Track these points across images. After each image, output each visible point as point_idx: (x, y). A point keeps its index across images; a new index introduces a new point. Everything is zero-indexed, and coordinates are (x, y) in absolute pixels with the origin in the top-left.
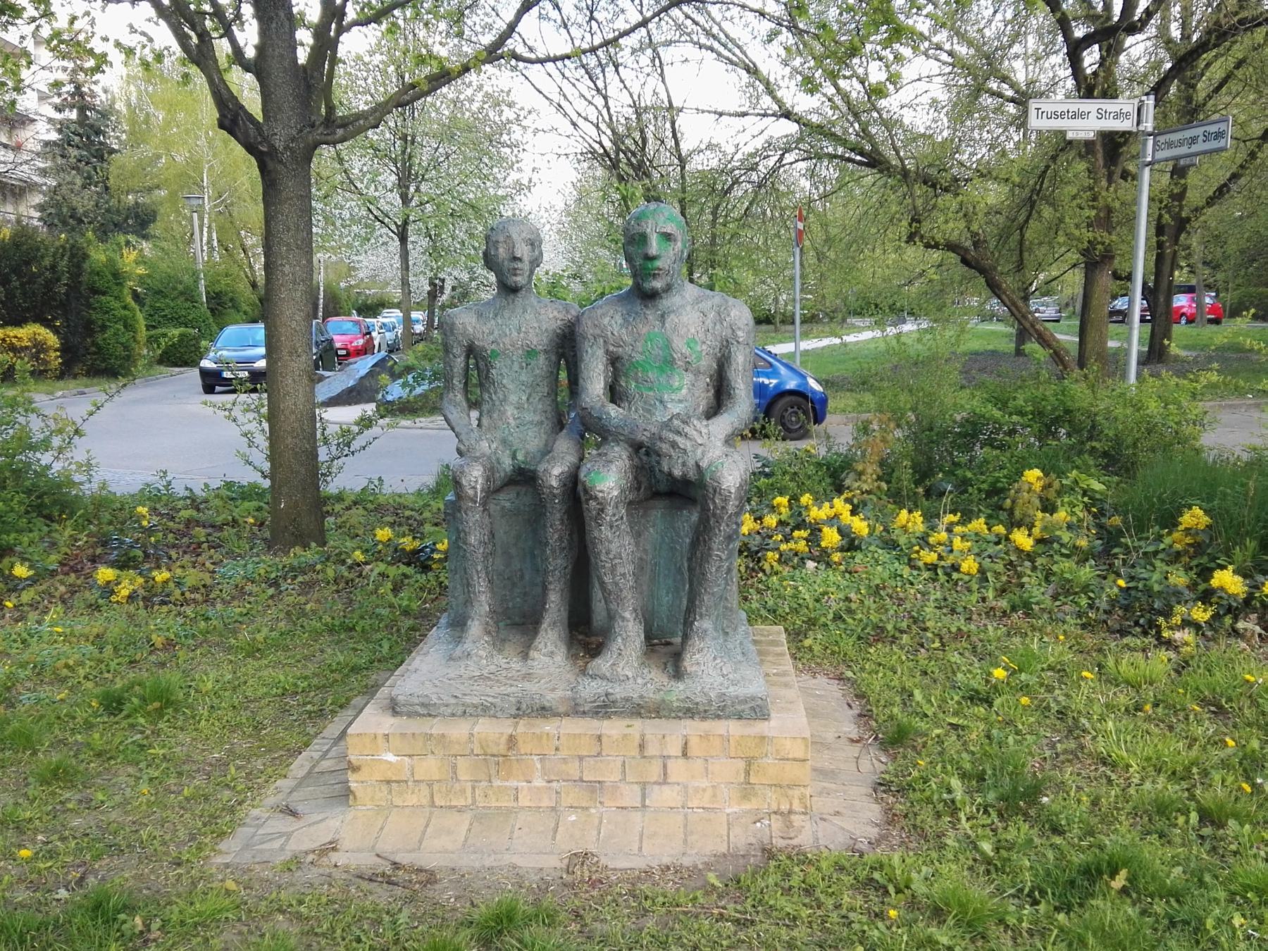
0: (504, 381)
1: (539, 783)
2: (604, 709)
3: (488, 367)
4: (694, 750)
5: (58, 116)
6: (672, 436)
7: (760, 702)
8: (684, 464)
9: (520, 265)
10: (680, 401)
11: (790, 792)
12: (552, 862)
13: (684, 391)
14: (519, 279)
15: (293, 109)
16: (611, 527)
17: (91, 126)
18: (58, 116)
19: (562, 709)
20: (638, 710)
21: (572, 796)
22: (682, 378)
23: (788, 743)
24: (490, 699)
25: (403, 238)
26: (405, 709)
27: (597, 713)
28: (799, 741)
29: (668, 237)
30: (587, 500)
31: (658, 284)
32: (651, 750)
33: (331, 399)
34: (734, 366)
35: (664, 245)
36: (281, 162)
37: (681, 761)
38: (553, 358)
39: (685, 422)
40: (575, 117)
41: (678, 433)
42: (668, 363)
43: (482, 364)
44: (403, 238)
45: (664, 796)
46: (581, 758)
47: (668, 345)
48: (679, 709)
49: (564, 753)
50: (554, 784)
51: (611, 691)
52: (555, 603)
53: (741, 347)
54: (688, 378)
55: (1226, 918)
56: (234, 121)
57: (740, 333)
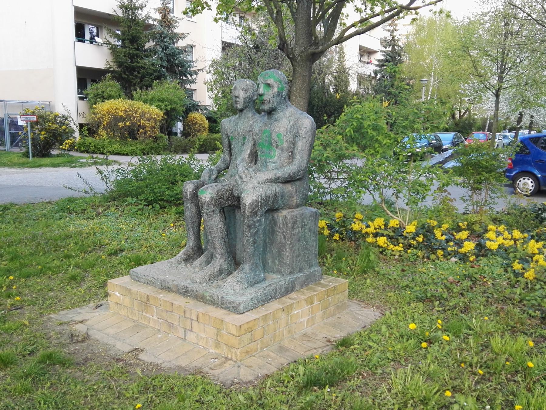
1: (155, 318)
4: (201, 320)
5: (384, 49)
9: (238, 100)
10: (274, 163)
11: (232, 350)
12: (122, 347)
13: (276, 158)
14: (238, 105)
15: (304, 39)
16: (207, 215)
17: (396, 53)
18: (384, 49)
19: (174, 290)
21: (164, 328)
22: (275, 152)
23: (230, 325)
25: (497, 96)
27: (185, 294)
28: (234, 326)
29: (269, 85)
32: (188, 315)
36: (296, 62)
37: (196, 322)
44: (497, 96)
45: (191, 337)
46: (167, 311)
47: (270, 136)
48: (208, 300)
49: (162, 308)
50: (159, 320)
54: (278, 152)
56: (283, 46)
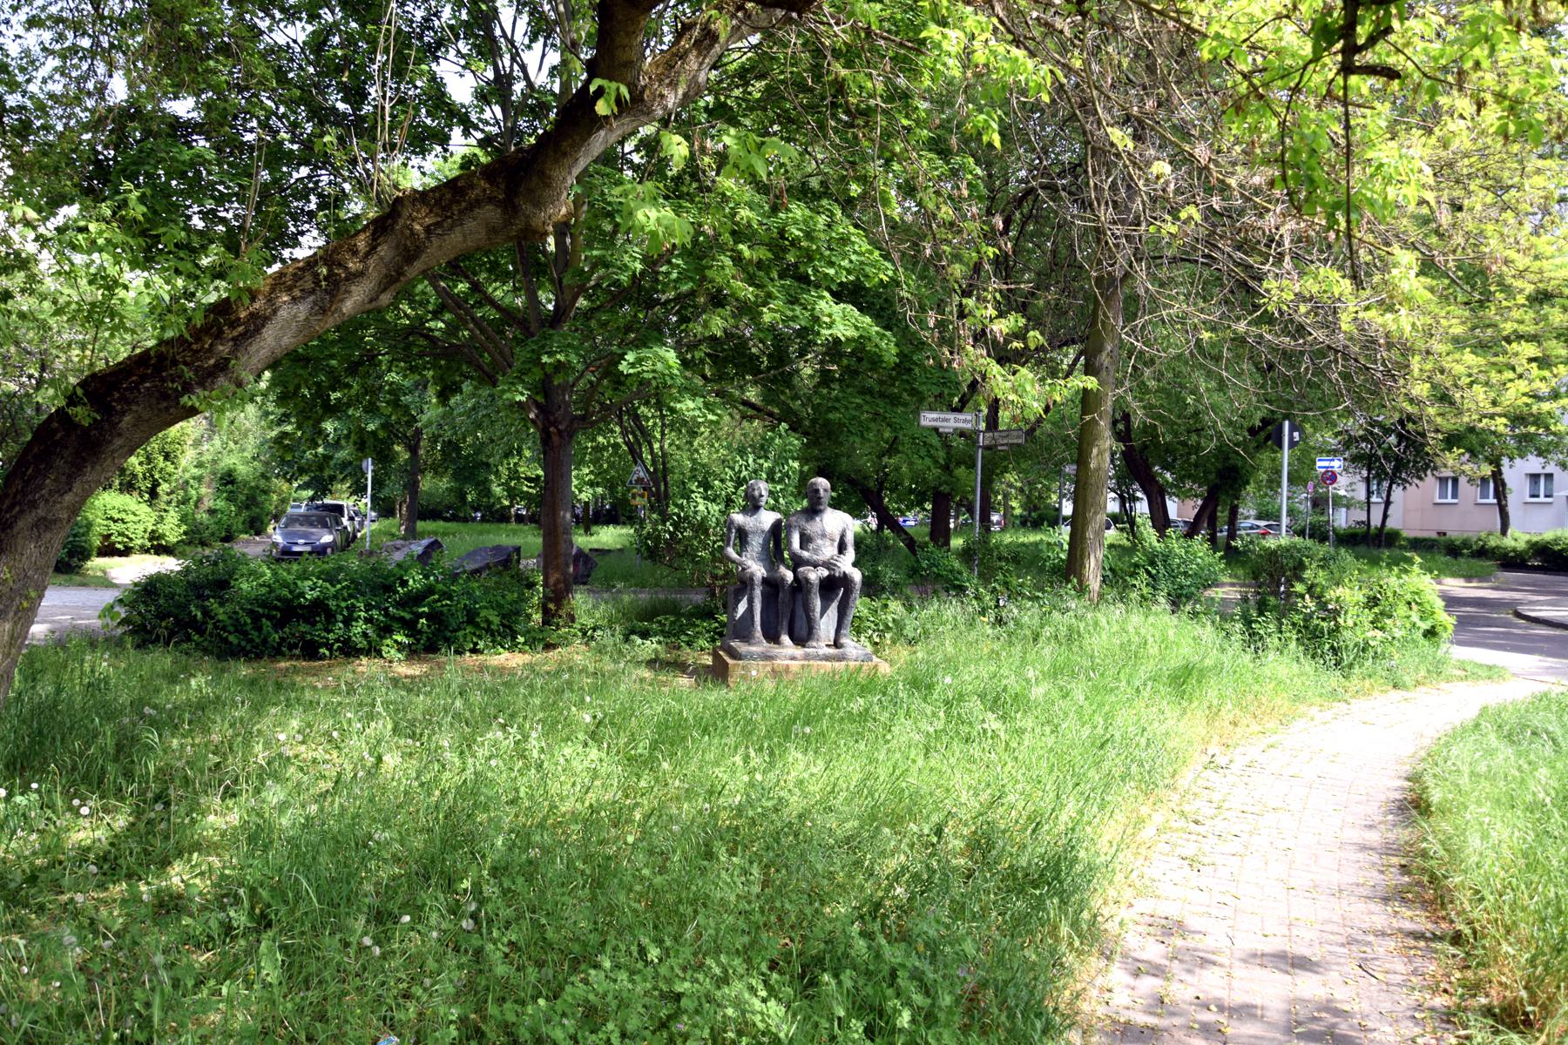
20: (827, 658)
42: (824, 536)
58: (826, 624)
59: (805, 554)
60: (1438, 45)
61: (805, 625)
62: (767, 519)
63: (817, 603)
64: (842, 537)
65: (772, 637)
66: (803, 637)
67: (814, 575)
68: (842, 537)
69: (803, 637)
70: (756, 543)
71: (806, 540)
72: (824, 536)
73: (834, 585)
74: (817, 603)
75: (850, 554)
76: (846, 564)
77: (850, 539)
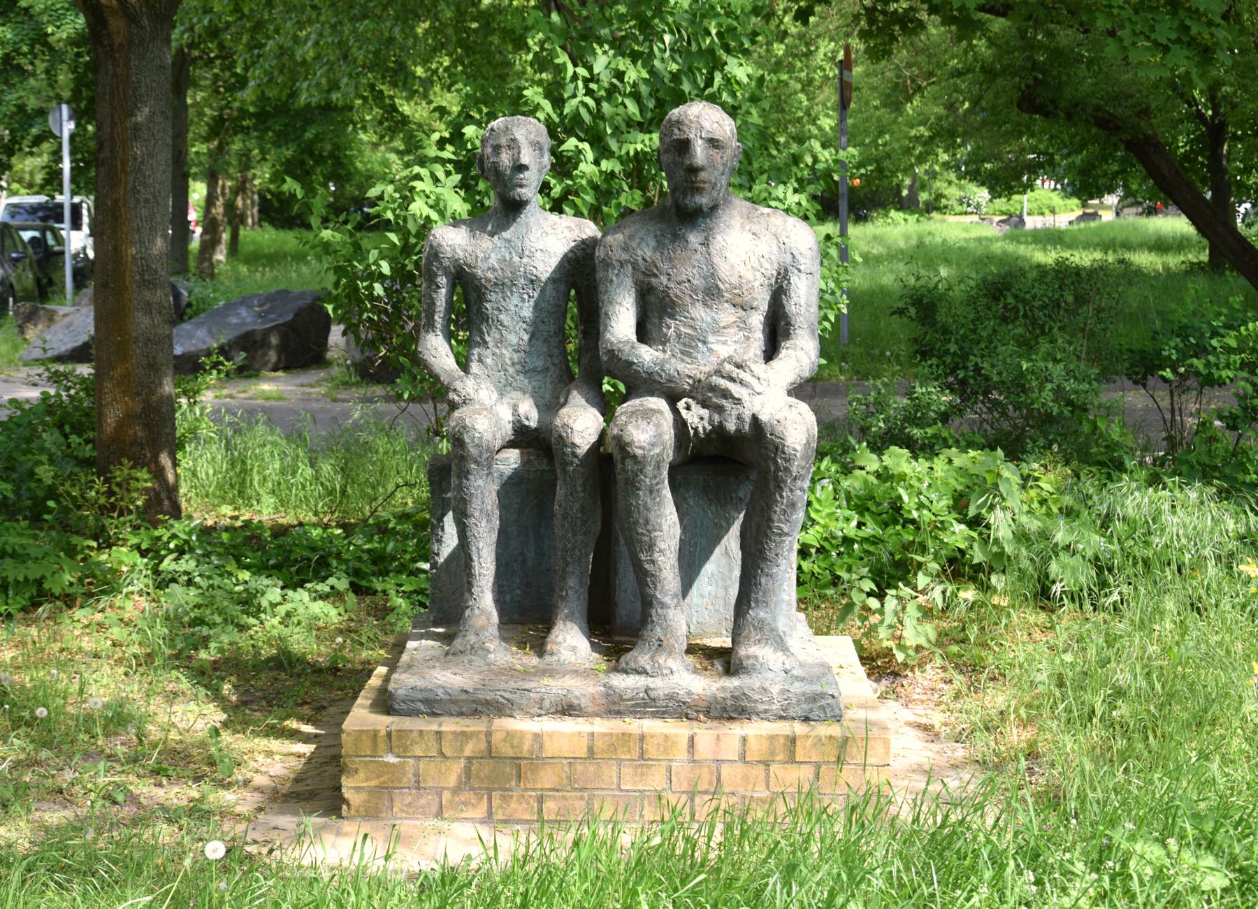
0: (502, 317)
2: (647, 706)
3: (481, 298)
6: (723, 383)
7: (830, 701)
8: (739, 418)
20: (682, 709)
24: (507, 695)
26: (404, 706)
30: (623, 459)
31: (704, 200)
33: (75, 350)
34: (795, 299)
35: (713, 152)
38: (562, 288)
39: (739, 366)
40: (1176, 407)
41: (732, 380)
42: (712, 293)
43: (473, 296)
51: (652, 686)
52: (574, 590)
53: (803, 276)
55: (1077, 412)
57: (802, 260)
58: (697, 605)
59: (647, 355)
60: (1123, 33)
61: (631, 576)
62: (549, 238)
63: (666, 523)
64: (779, 293)
65: (528, 619)
66: (619, 626)
67: (649, 429)
68: (779, 293)
69: (619, 626)
70: (514, 315)
71: (654, 312)
72: (712, 293)
73: (729, 469)
74: (666, 523)
75: (802, 354)
76: (773, 398)
77: (803, 298)
